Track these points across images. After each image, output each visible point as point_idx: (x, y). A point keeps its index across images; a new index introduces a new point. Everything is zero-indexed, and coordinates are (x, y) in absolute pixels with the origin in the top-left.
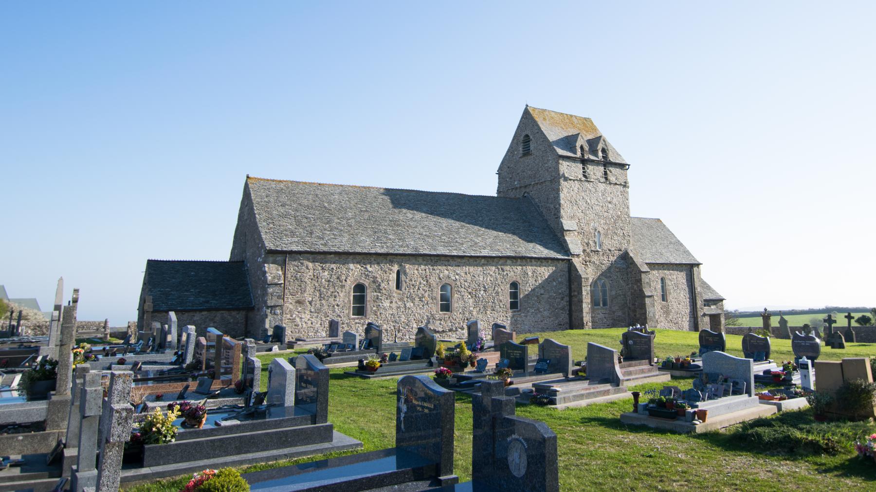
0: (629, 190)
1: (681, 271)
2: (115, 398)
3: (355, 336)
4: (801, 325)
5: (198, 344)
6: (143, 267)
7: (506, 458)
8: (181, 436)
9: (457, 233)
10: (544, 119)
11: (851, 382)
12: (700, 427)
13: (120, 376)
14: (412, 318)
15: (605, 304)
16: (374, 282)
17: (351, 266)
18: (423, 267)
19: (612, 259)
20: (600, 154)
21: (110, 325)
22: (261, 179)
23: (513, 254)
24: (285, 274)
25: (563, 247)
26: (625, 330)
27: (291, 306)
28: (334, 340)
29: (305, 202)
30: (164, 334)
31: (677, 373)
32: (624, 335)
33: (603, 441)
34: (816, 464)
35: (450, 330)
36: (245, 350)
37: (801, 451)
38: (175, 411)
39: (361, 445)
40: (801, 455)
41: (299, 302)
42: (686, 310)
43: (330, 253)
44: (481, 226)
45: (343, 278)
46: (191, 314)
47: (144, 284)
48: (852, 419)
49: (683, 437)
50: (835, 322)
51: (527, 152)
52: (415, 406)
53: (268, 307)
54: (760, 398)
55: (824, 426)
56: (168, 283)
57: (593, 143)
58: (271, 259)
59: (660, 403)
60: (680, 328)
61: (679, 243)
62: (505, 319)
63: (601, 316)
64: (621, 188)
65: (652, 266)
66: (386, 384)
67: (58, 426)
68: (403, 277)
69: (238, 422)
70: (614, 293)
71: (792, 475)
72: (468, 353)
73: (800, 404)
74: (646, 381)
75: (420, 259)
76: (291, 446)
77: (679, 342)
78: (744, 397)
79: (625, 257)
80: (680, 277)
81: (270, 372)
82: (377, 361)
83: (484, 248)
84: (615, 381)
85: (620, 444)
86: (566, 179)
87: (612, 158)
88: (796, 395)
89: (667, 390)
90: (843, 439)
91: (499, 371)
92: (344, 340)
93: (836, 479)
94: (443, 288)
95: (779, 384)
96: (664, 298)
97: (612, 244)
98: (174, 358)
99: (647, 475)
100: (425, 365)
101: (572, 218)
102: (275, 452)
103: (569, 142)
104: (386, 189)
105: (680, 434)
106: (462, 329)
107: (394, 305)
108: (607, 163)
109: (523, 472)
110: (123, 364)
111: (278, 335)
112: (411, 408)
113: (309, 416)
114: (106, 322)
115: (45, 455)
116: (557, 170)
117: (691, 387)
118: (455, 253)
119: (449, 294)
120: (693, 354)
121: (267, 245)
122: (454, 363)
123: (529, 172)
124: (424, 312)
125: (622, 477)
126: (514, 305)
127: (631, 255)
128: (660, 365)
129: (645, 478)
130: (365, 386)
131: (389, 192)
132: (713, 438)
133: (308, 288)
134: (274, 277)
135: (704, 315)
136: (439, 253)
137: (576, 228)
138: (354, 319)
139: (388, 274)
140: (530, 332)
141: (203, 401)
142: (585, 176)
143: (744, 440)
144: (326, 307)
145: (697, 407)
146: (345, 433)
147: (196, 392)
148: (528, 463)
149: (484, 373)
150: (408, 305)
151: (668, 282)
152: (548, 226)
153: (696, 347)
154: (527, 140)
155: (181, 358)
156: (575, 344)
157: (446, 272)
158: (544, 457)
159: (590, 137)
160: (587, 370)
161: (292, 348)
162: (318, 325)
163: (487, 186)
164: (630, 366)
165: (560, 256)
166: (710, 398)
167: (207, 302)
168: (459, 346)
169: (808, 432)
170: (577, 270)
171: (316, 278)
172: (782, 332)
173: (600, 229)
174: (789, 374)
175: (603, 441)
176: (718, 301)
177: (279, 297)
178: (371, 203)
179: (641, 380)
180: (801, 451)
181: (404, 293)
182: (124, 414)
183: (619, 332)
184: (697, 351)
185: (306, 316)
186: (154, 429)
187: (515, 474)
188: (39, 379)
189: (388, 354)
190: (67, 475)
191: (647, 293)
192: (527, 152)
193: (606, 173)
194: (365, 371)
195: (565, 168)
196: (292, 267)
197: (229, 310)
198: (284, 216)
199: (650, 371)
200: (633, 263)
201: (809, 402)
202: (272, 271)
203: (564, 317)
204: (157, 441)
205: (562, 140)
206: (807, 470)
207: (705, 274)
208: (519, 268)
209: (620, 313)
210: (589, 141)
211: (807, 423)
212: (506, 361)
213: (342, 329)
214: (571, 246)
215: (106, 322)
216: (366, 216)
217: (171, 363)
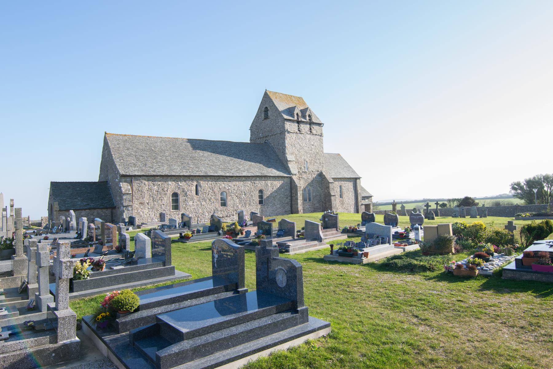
0: (324, 138)
1: (350, 182)
2: (62, 256)
3: (176, 221)
4: (412, 209)
5: (89, 227)
6: (49, 186)
7: (275, 278)
8: (92, 275)
9: (229, 163)
10: (276, 98)
11: (442, 235)
12: (365, 260)
13: (63, 244)
14: (205, 210)
15: (310, 200)
16: (183, 191)
17: (170, 183)
18: (210, 182)
19: (314, 176)
20: (308, 118)
21: (31, 219)
22: (114, 134)
23: (260, 175)
24: (132, 188)
25: (286, 170)
26: (323, 213)
27: (137, 206)
28: (163, 223)
29: (141, 147)
30: (68, 223)
31: (350, 235)
32: (323, 216)
33: (316, 269)
34: (424, 276)
35: (227, 216)
36: (119, 229)
37: (417, 270)
38: (88, 263)
39: (191, 276)
40: (417, 272)
41: (141, 203)
42: (353, 202)
43: (158, 176)
44: (242, 159)
45: (166, 189)
46: (80, 211)
47: (50, 195)
48: (441, 254)
49: (357, 266)
50: (430, 206)
51: (266, 117)
52: (223, 255)
53: (124, 207)
54: (395, 245)
55: (428, 258)
56: (64, 194)
57: (304, 112)
58: (123, 180)
59: (345, 250)
60: (349, 212)
61: (349, 167)
62: (257, 209)
63: (308, 206)
64: (319, 137)
65: (335, 179)
66: (195, 245)
67: (20, 273)
68: (199, 188)
69: (123, 267)
70: (314, 194)
71: (413, 282)
72: (239, 228)
73: (415, 247)
74: (335, 239)
75: (208, 178)
76: (153, 278)
77: (349, 219)
78: (387, 245)
79: (321, 175)
80: (350, 185)
81: (136, 241)
82: (190, 233)
83: (244, 172)
84: (319, 239)
85: (325, 270)
86: (289, 132)
87: (314, 120)
88: (412, 243)
89: (348, 243)
90: (437, 264)
91: (257, 236)
92: (170, 223)
93: (434, 283)
94: (222, 194)
95: (402, 238)
96: (341, 196)
97: (314, 169)
98: (76, 236)
99: (341, 284)
100: (216, 235)
101: (292, 154)
102: (145, 282)
103: (290, 111)
104: (188, 140)
105: (355, 264)
106: (233, 215)
107: (195, 204)
108: (311, 123)
109: (284, 284)
110: (47, 239)
111: (131, 222)
112: (220, 256)
113: (161, 262)
114: (29, 217)
115: (17, 288)
116: (284, 127)
117: (360, 241)
118: (228, 175)
119: (225, 197)
120: (358, 225)
121: (120, 172)
122: (232, 233)
123: (268, 129)
124: (211, 207)
125: (328, 286)
126: (261, 202)
127: (324, 174)
128: (341, 231)
129: (340, 286)
130: (185, 247)
131: (190, 141)
132: (372, 266)
133: (146, 196)
134: (126, 190)
135: (362, 205)
136: (219, 174)
139: (190, 187)
140: (270, 216)
141: (102, 257)
142: (299, 130)
143: (388, 266)
144: (157, 206)
145: (363, 251)
146: (180, 270)
147: (94, 253)
148: (287, 280)
149: (250, 238)
150: (203, 203)
151: (343, 188)
152: (279, 158)
153: (359, 221)
154: (266, 110)
155: (80, 235)
156: (298, 221)
157: (223, 185)
158: (296, 276)
159: (302, 108)
160: (305, 234)
161: (140, 228)
162: (153, 215)
163: (245, 137)
164: (326, 232)
165: (285, 175)
166: (370, 246)
167: (88, 205)
168: (234, 224)
169: (421, 261)
170: (295, 182)
171: (150, 190)
172: (402, 213)
173: (307, 160)
174: (408, 233)
175: (316, 269)
176: (369, 197)
177: (130, 201)
178: (179, 147)
179: (333, 239)
180: (417, 270)
181: (200, 197)
182: (69, 264)
183: (320, 215)
184: (360, 223)
185: (146, 211)
186: (77, 272)
187: (280, 286)
188: (4, 249)
189: (196, 229)
190: (32, 297)
191: (332, 194)
192: (266, 117)
193: (310, 129)
194: (183, 239)
195: (288, 126)
196: (136, 184)
197: (101, 209)
198: (129, 155)
199: (336, 234)
200: (325, 178)
201: (420, 246)
202: (125, 187)
203: (288, 208)
204: (80, 278)
205: (286, 110)
206: (420, 279)
207: (363, 183)
208: (264, 182)
209: (318, 205)
210: (301, 111)
211: (419, 257)
212: (261, 231)
213: (167, 218)
214: (291, 169)
215: (29, 217)
216: (177, 154)
217: (75, 238)
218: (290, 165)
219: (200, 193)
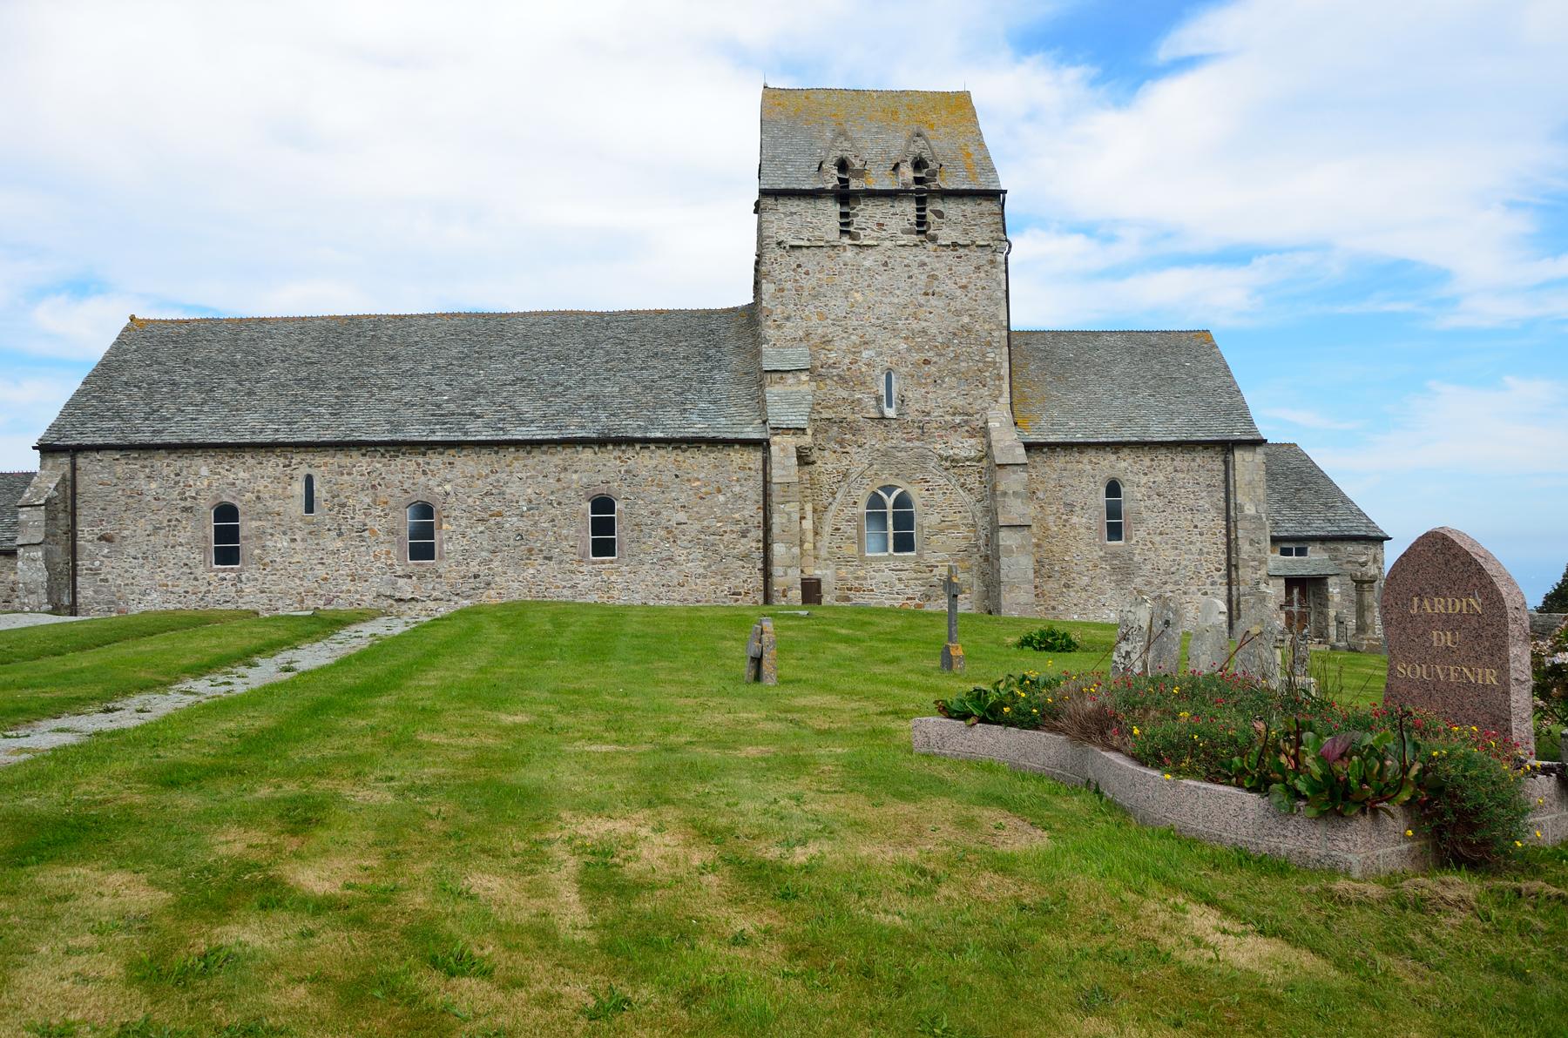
193: (921, 221)
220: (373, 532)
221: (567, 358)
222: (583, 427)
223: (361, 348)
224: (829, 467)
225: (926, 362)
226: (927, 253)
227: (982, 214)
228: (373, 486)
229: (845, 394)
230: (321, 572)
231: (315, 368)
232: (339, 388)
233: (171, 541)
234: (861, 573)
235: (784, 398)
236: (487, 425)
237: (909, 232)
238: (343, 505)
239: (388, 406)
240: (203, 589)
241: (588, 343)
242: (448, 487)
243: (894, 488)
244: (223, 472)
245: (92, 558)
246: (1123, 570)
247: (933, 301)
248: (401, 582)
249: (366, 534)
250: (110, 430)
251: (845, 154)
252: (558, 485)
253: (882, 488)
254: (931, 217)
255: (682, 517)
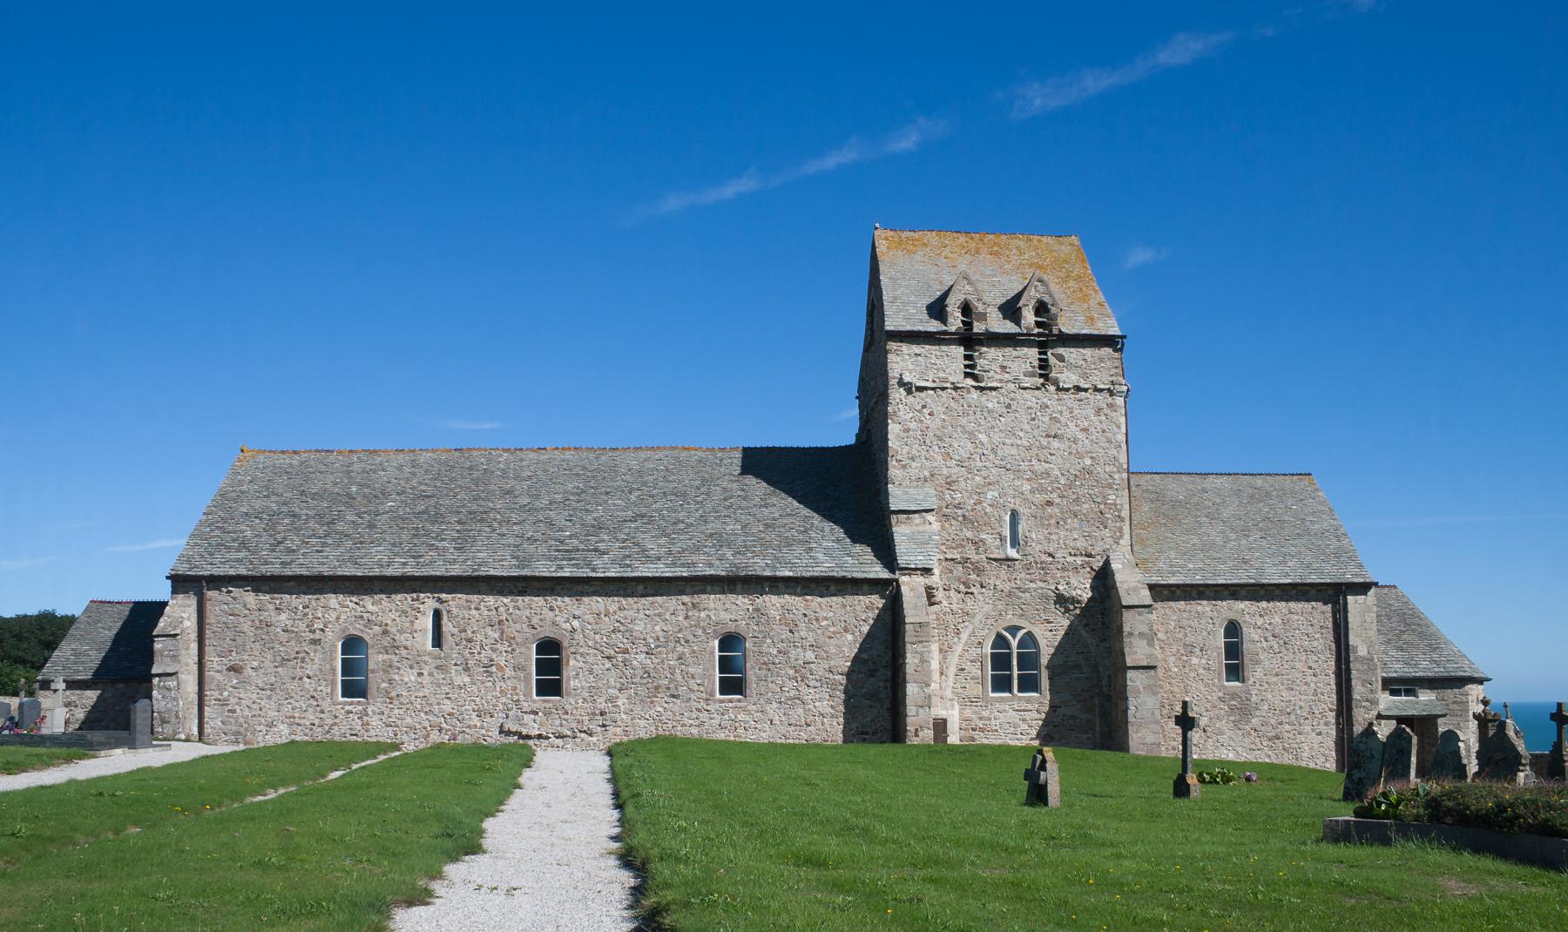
25: (886, 552)
41: (233, 669)
65: (1162, 592)
68: (447, 627)
107: (426, 679)
137: (932, 503)
138: (345, 704)
193: (1044, 365)
218: (902, 533)
219: (448, 641)
220: (500, 668)
221: (684, 494)
222: (710, 565)
223: (476, 482)
224: (954, 607)
225: (1049, 503)
226: (1049, 396)
227: (1101, 360)
228: (500, 622)
229: (969, 534)
230: (448, 707)
231: (432, 501)
232: (459, 522)
233: (299, 673)
234: (985, 714)
235: (910, 538)
236: (613, 561)
237: (1032, 375)
238: (470, 641)
239: (511, 541)
240: (329, 721)
241: (704, 480)
242: (576, 623)
243: (1019, 628)
244: (352, 605)
245: (221, 689)
246: (1242, 711)
247: (1055, 444)
248: (528, 718)
249: (494, 669)
250: (239, 561)
251: (970, 298)
252: (686, 623)
253: (1007, 629)
254: (1052, 360)
255: (810, 655)
